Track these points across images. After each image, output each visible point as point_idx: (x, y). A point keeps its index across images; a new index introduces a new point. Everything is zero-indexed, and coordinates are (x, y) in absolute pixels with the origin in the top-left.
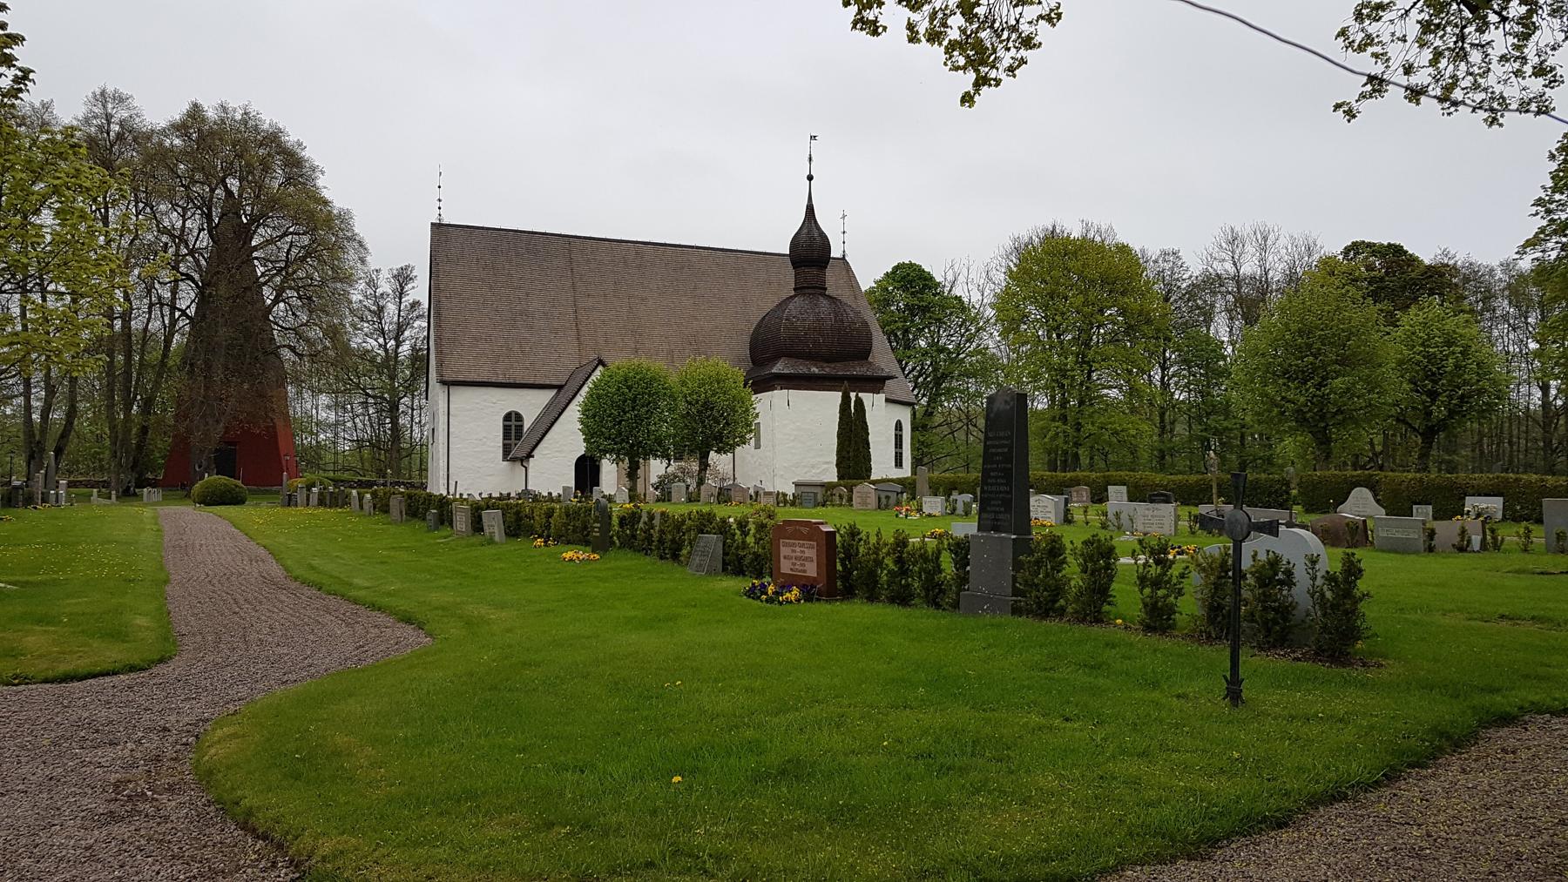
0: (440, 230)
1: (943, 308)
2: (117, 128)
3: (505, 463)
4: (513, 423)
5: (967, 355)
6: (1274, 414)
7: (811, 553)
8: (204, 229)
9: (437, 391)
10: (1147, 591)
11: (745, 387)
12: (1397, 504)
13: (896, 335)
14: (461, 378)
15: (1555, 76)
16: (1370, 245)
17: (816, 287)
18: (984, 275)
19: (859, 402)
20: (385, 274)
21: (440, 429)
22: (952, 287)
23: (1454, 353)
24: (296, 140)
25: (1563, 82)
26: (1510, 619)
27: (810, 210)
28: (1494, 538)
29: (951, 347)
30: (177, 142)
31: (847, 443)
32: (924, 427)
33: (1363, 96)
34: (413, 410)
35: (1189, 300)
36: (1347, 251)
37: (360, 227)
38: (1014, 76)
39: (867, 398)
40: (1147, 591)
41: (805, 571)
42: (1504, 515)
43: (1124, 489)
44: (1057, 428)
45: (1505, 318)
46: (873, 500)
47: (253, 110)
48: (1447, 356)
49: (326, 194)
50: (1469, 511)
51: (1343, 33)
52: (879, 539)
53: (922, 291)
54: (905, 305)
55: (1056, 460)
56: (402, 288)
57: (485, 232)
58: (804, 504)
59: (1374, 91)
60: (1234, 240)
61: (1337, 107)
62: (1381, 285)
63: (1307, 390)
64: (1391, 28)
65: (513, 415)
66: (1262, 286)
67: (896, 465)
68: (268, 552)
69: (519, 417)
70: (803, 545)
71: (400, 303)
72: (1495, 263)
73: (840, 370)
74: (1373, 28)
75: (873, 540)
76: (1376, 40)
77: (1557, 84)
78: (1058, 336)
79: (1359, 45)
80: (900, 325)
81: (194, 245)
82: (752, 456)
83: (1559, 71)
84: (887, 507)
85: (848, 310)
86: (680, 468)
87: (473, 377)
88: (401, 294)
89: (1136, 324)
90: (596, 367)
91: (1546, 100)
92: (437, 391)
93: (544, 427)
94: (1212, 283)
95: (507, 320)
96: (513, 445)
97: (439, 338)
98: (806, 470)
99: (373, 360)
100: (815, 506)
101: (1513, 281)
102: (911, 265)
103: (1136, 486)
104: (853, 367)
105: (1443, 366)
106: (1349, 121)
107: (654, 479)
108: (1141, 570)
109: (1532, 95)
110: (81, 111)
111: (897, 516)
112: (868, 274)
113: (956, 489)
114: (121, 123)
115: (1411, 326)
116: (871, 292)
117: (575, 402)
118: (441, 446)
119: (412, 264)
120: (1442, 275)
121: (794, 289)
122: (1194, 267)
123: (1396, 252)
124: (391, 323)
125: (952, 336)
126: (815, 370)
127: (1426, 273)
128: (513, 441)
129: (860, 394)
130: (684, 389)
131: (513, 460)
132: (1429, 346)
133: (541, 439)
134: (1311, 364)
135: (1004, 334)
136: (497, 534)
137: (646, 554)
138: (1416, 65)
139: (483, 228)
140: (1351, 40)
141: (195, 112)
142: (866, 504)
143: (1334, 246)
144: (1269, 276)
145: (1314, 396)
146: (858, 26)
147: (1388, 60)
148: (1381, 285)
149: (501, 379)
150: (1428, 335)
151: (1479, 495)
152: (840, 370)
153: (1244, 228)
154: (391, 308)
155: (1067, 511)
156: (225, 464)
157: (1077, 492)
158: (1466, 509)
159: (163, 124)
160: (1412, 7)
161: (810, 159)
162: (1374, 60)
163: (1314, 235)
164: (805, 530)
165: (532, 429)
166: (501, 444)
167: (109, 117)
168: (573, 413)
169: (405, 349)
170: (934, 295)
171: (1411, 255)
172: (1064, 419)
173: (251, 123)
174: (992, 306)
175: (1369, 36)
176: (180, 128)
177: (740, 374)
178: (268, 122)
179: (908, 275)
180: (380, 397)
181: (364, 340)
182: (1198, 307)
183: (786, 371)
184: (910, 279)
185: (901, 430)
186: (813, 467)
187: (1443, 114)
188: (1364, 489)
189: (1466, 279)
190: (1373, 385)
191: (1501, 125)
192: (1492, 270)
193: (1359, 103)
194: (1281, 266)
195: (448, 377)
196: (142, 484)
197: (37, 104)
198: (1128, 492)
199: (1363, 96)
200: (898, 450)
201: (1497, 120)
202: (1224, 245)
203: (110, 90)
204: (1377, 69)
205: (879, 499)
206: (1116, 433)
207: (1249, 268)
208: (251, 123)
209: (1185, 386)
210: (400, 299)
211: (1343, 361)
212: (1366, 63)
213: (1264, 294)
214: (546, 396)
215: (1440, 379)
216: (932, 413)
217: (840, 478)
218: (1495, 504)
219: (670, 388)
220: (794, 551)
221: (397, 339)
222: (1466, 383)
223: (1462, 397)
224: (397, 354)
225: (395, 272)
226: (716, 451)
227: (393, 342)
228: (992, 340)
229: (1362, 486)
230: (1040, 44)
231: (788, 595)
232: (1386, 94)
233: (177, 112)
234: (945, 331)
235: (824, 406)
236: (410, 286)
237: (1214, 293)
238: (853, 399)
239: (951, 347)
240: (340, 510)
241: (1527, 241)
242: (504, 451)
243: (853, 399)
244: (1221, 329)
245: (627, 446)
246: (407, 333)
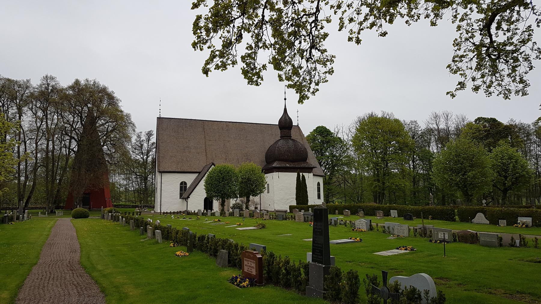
0: (160, 119)
1: (334, 142)
2: (51, 88)
4: (183, 185)
5: (343, 158)
6: (448, 185)
7: (254, 265)
8: (79, 122)
9: (158, 175)
10: (370, 295)
11: (262, 173)
12: (494, 220)
13: (318, 151)
14: (166, 170)
15: (526, 83)
16: (484, 118)
17: (288, 136)
18: (348, 130)
19: (303, 176)
20: (143, 133)
21: (158, 188)
22: (337, 134)
23: (512, 162)
25: (530, 85)
26: (521, 293)
27: (285, 110)
28: (524, 242)
29: (337, 155)
30: (71, 92)
32: (329, 183)
33: (457, 89)
34: (152, 179)
35: (421, 138)
36: (476, 121)
37: (133, 119)
38: (315, 95)
39: (306, 175)
40: (370, 295)
41: (252, 272)
42: (532, 224)
43: (396, 211)
44: (376, 184)
45: (535, 142)
46: (302, 218)
47: (97, 81)
48: (510, 163)
49: (122, 109)
50: (519, 223)
51: (449, 66)
52: (280, 259)
53: (326, 136)
54: (321, 141)
55: (376, 195)
56: (149, 138)
57: (175, 120)
58: (279, 219)
59: (461, 87)
60: (436, 117)
61: (448, 93)
62: (488, 132)
63: (459, 176)
64: (466, 64)
65: (183, 183)
66: (447, 132)
67: (318, 198)
68: (80, 247)
69: (185, 183)
70: (251, 262)
71: (148, 143)
72: (530, 123)
73: (297, 165)
74: (460, 65)
75: (278, 259)
76: (461, 69)
77: (528, 86)
78: (375, 151)
79: (454, 71)
80: (319, 147)
81: (75, 127)
82: (267, 196)
83: (528, 82)
84: (307, 221)
85: (299, 144)
86: (241, 200)
87: (170, 170)
88: (149, 140)
89: (403, 147)
90: (211, 166)
91: (525, 91)
92: (158, 175)
93: (192, 189)
94: (430, 131)
95: (182, 150)
97: (159, 157)
98: (285, 201)
99: (139, 163)
100: (283, 220)
101: (537, 129)
102: (322, 127)
103: (400, 210)
104: (301, 164)
105: (509, 167)
106: (453, 98)
107: (231, 205)
108: (367, 287)
109: (520, 89)
110: (39, 83)
111: (310, 225)
112: (307, 130)
113: (337, 209)
114: (52, 86)
115: (496, 152)
116: (309, 136)
117: (203, 179)
118: (158, 194)
119: (153, 130)
120: (510, 129)
121: (280, 137)
122: (422, 126)
123: (493, 121)
124: (145, 150)
125: (338, 151)
126: (288, 165)
127: (505, 128)
129: (304, 174)
130: (241, 174)
131: (183, 198)
132: (503, 160)
134: (460, 167)
135: (356, 150)
136: (159, 240)
137: (206, 253)
138: (476, 78)
139: (174, 118)
140: (452, 69)
141: (77, 82)
142: (300, 220)
143: (471, 118)
144: (449, 129)
145: (462, 178)
146: (250, 83)
147: (466, 76)
148: (488, 132)
149: (179, 170)
150: (502, 155)
151: (523, 217)
152: (297, 165)
153: (440, 112)
154: (145, 145)
155: (371, 225)
156: (86, 202)
157: (379, 213)
158: (518, 222)
159: (66, 86)
160: (473, 57)
161: (285, 93)
162: (461, 76)
164: (252, 256)
165: (190, 187)
167: (48, 84)
168: (202, 183)
169: (150, 159)
170: (331, 137)
171: (499, 122)
172: (378, 181)
173: (96, 85)
174: (351, 141)
175: (458, 68)
176: (72, 88)
177: (260, 168)
178: (102, 85)
179: (321, 130)
180: (141, 176)
181: (136, 156)
182: (425, 140)
183: (278, 166)
184: (322, 131)
185: (319, 185)
186: (288, 200)
187: (486, 97)
188: (481, 213)
189: (520, 129)
190: (484, 175)
191: (510, 99)
192: (529, 125)
193: (456, 92)
194: (453, 126)
195: (161, 170)
196: (58, 208)
197: (25, 80)
198: (398, 213)
199: (457, 89)
200: (319, 193)
201: (508, 97)
202: (433, 118)
203: (49, 75)
204: (462, 79)
205: (305, 217)
206: (397, 186)
207: (442, 126)
208: (96, 85)
209: (422, 168)
210: (148, 141)
211: (472, 166)
212: (458, 78)
213: (448, 135)
214: (194, 176)
215: (508, 172)
216: (332, 178)
217: (297, 204)
218: (528, 220)
219: (236, 174)
220: (248, 263)
221: (147, 155)
222: (517, 173)
223: (516, 178)
224: (147, 160)
225: (147, 133)
226: (252, 196)
227: (146, 156)
228: (351, 152)
229: (480, 212)
230: (328, 81)
231: (244, 283)
232: (465, 88)
233: (71, 82)
234: (335, 149)
235: (290, 178)
236: (152, 137)
237: (430, 135)
238: (301, 176)
239: (337, 155)
240: (116, 223)
241: (539, 118)
242: (180, 196)
243: (301, 176)
244: (433, 148)
245: (220, 195)
246: (150, 153)
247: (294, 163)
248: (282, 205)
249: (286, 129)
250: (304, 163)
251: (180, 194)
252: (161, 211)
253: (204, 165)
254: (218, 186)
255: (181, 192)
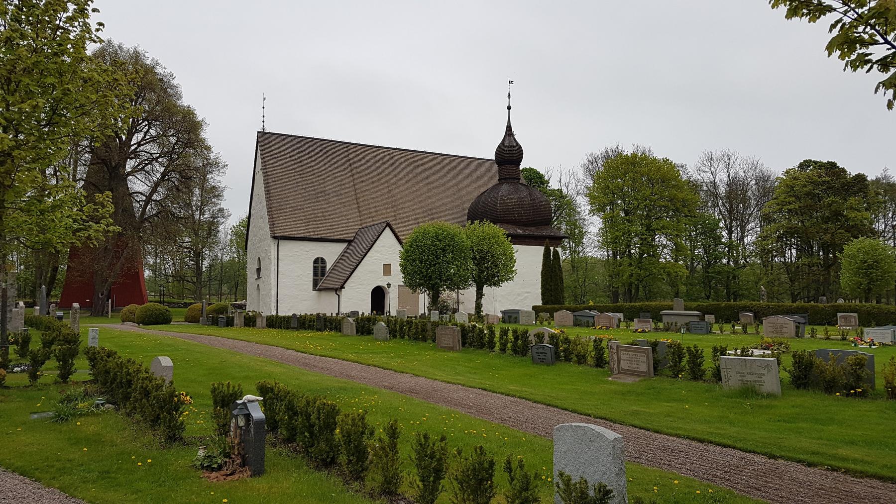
0: (264, 138)
3: (315, 292)
4: (320, 265)
14: (286, 235)
16: (815, 162)
24: (169, 72)
27: (509, 128)
31: (549, 280)
69: (323, 261)
96: (319, 280)
98: (515, 297)
118: (272, 280)
128: (320, 277)
131: (320, 290)
133: (350, 276)
139: (291, 136)
149: (312, 235)
163: (756, 158)
166: (312, 279)
186: (519, 295)
195: (279, 233)
247: (529, 228)
248: (510, 304)
249: (511, 164)
250: (547, 229)
251: (313, 282)
252: (277, 312)
253: (357, 228)
254: (434, 265)
255: (315, 278)
